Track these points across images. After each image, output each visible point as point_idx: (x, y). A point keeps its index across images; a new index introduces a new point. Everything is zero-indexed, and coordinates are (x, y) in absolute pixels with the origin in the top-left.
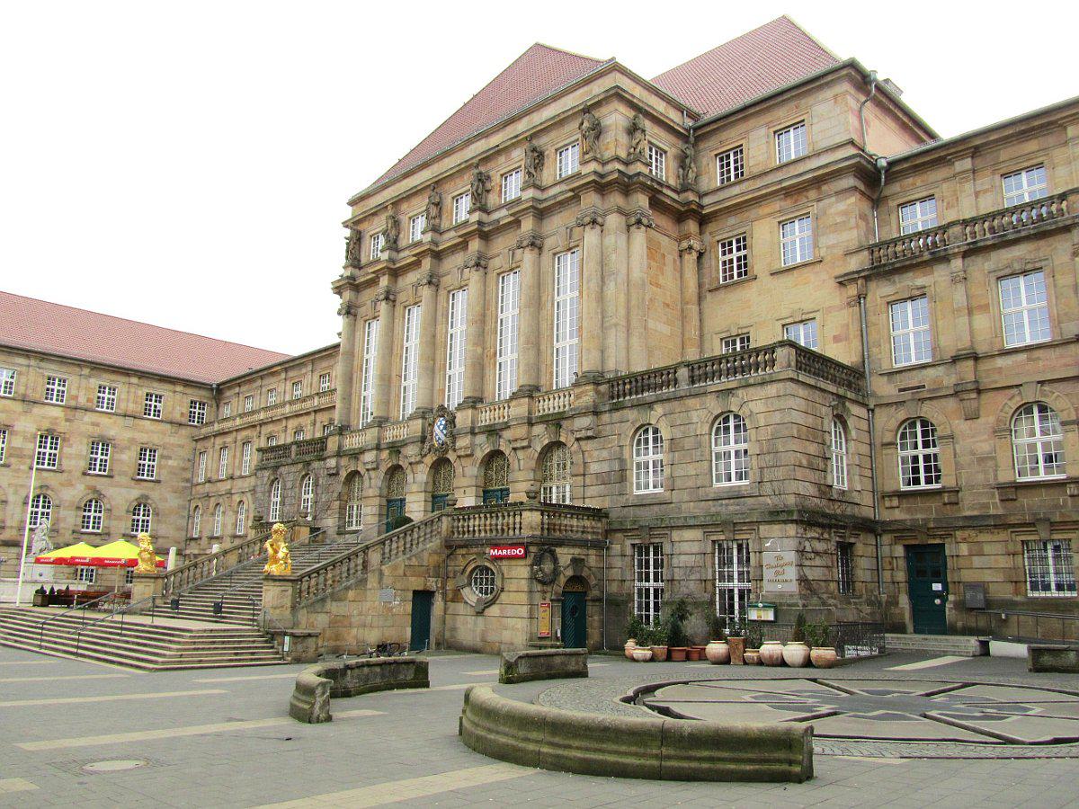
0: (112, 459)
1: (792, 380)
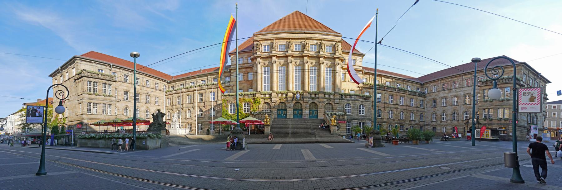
0: (150, 100)
1: (81, 73)
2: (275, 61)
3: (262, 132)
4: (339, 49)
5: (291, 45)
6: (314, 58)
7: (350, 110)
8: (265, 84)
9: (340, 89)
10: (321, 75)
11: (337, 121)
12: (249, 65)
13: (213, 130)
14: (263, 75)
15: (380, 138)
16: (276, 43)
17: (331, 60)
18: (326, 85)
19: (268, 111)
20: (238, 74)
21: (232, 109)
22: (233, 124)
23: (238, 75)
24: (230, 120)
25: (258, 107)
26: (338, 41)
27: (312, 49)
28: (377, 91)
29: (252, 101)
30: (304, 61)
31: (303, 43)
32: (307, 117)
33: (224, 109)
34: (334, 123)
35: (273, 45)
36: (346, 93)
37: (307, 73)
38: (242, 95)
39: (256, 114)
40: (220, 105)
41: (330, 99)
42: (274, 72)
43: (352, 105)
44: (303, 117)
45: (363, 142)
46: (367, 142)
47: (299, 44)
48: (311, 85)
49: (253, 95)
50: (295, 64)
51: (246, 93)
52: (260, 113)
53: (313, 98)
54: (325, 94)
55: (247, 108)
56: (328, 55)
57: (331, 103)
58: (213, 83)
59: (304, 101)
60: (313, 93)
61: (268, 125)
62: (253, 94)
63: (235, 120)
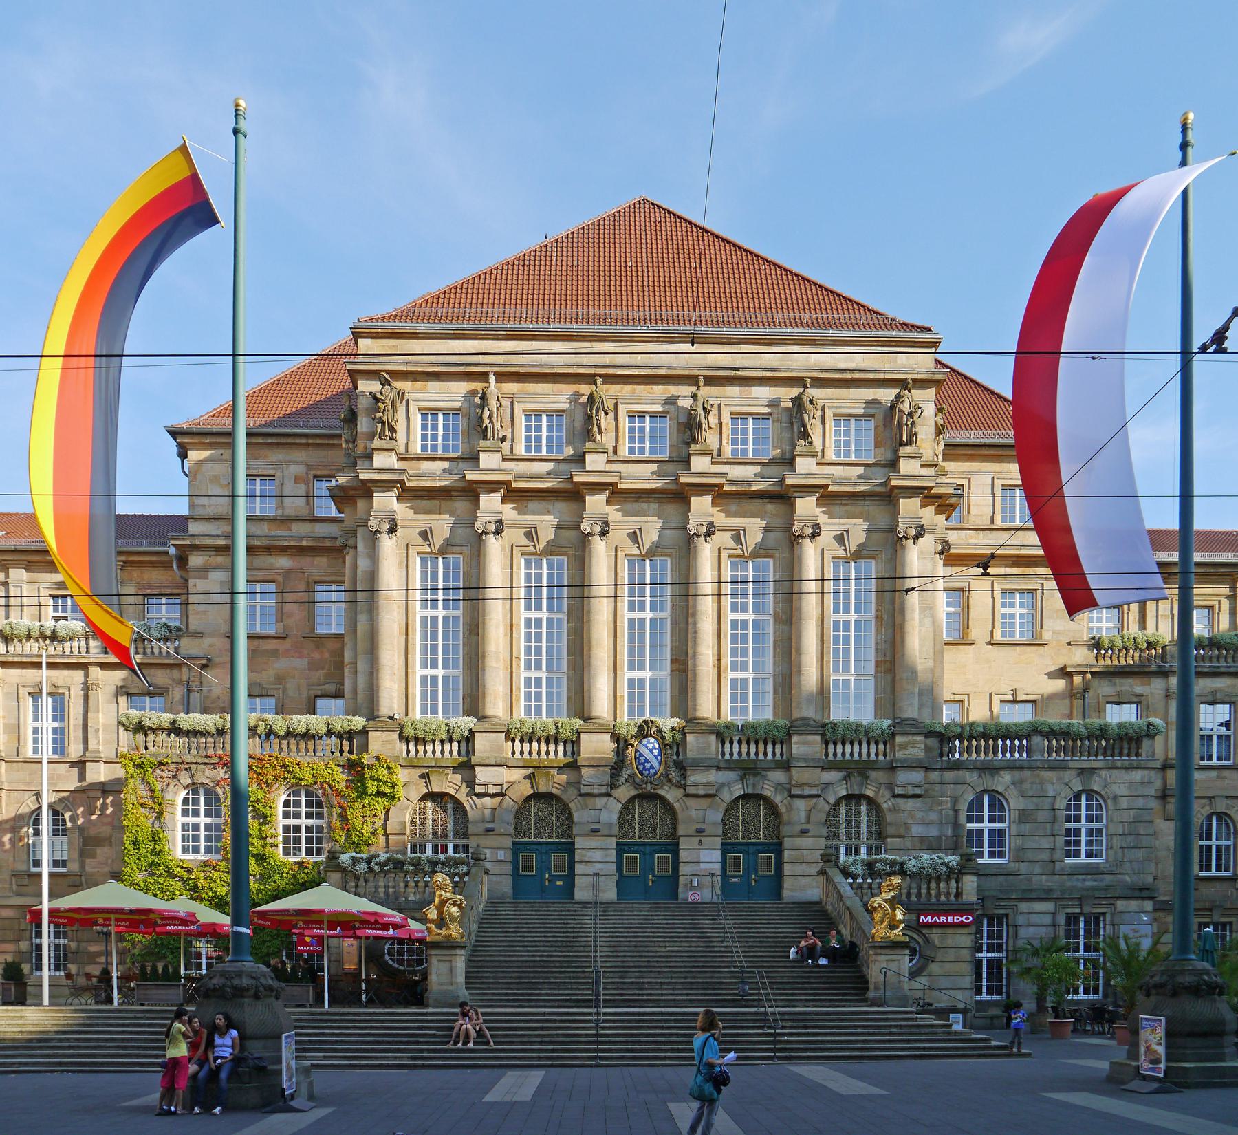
2: (500, 522)
3: (415, 993)
4: (925, 432)
5: (606, 421)
6: (755, 505)
7: (1001, 833)
8: (430, 673)
9: (930, 695)
10: (799, 610)
11: (914, 916)
12: (321, 529)
13: (57, 968)
14: (418, 612)
15: (1223, 1022)
16: (506, 403)
17: (870, 507)
18: (834, 676)
19: (451, 849)
20: (242, 585)
21: (196, 827)
22: (211, 932)
23: (241, 598)
24: (182, 905)
25: (379, 823)
26: (910, 376)
27: (745, 442)
28: (1201, 686)
29: (341, 777)
30: (692, 526)
31: (685, 403)
32: (706, 895)
33: (139, 820)
34: (892, 926)
35: (486, 413)
36: (972, 725)
37: (706, 606)
38: (270, 733)
39: (371, 870)
40: (104, 789)
41: (862, 769)
42: (491, 594)
43: (1015, 802)
44: (680, 890)
45: (1096, 1052)
46: (1120, 1053)
47: (653, 415)
48: (734, 682)
49: (350, 740)
50: (629, 543)
51: (301, 721)
52: (398, 865)
53: (748, 769)
54: (830, 733)
55: (309, 829)
56: (849, 477)
57: (870, 793)
58: (50, 624)
59: (691, 790)
60: (750, 733)
61: (448, 945)
62: (350, 735)
63: (220, 905)
